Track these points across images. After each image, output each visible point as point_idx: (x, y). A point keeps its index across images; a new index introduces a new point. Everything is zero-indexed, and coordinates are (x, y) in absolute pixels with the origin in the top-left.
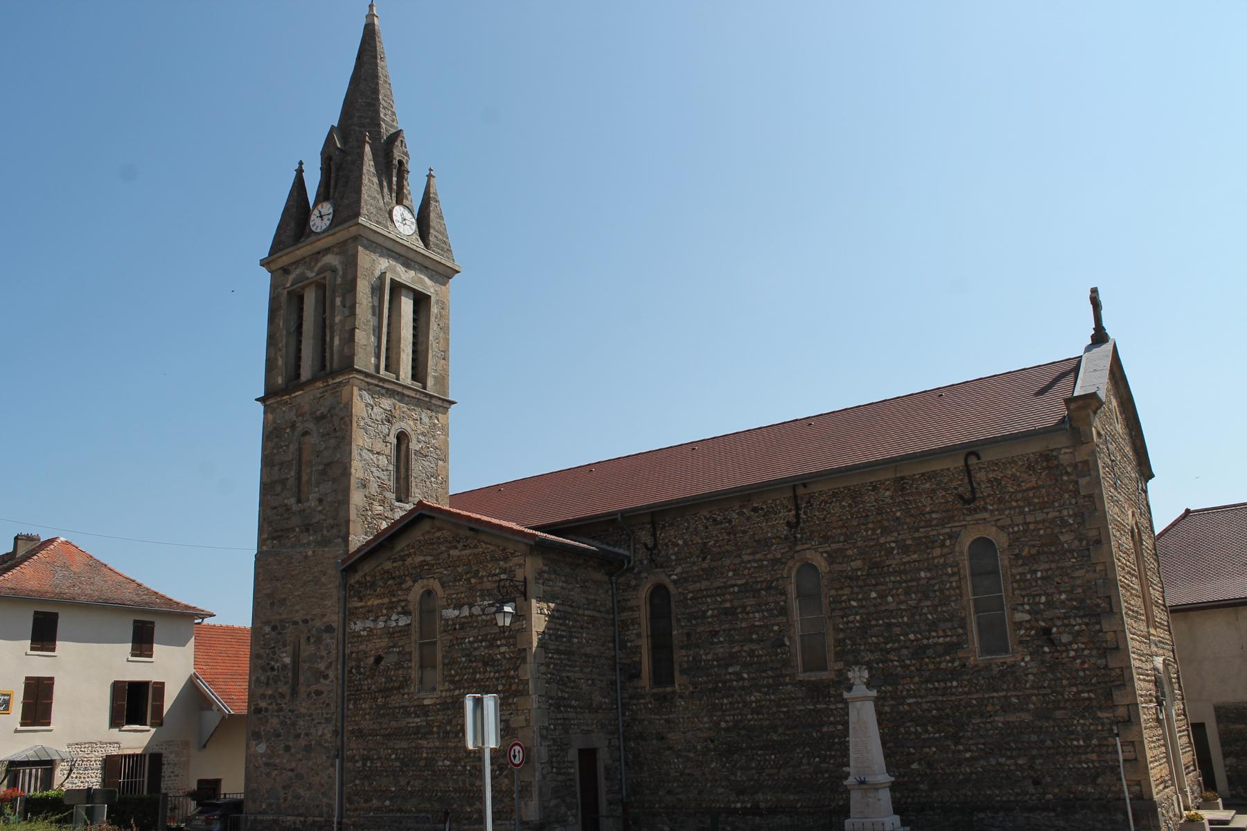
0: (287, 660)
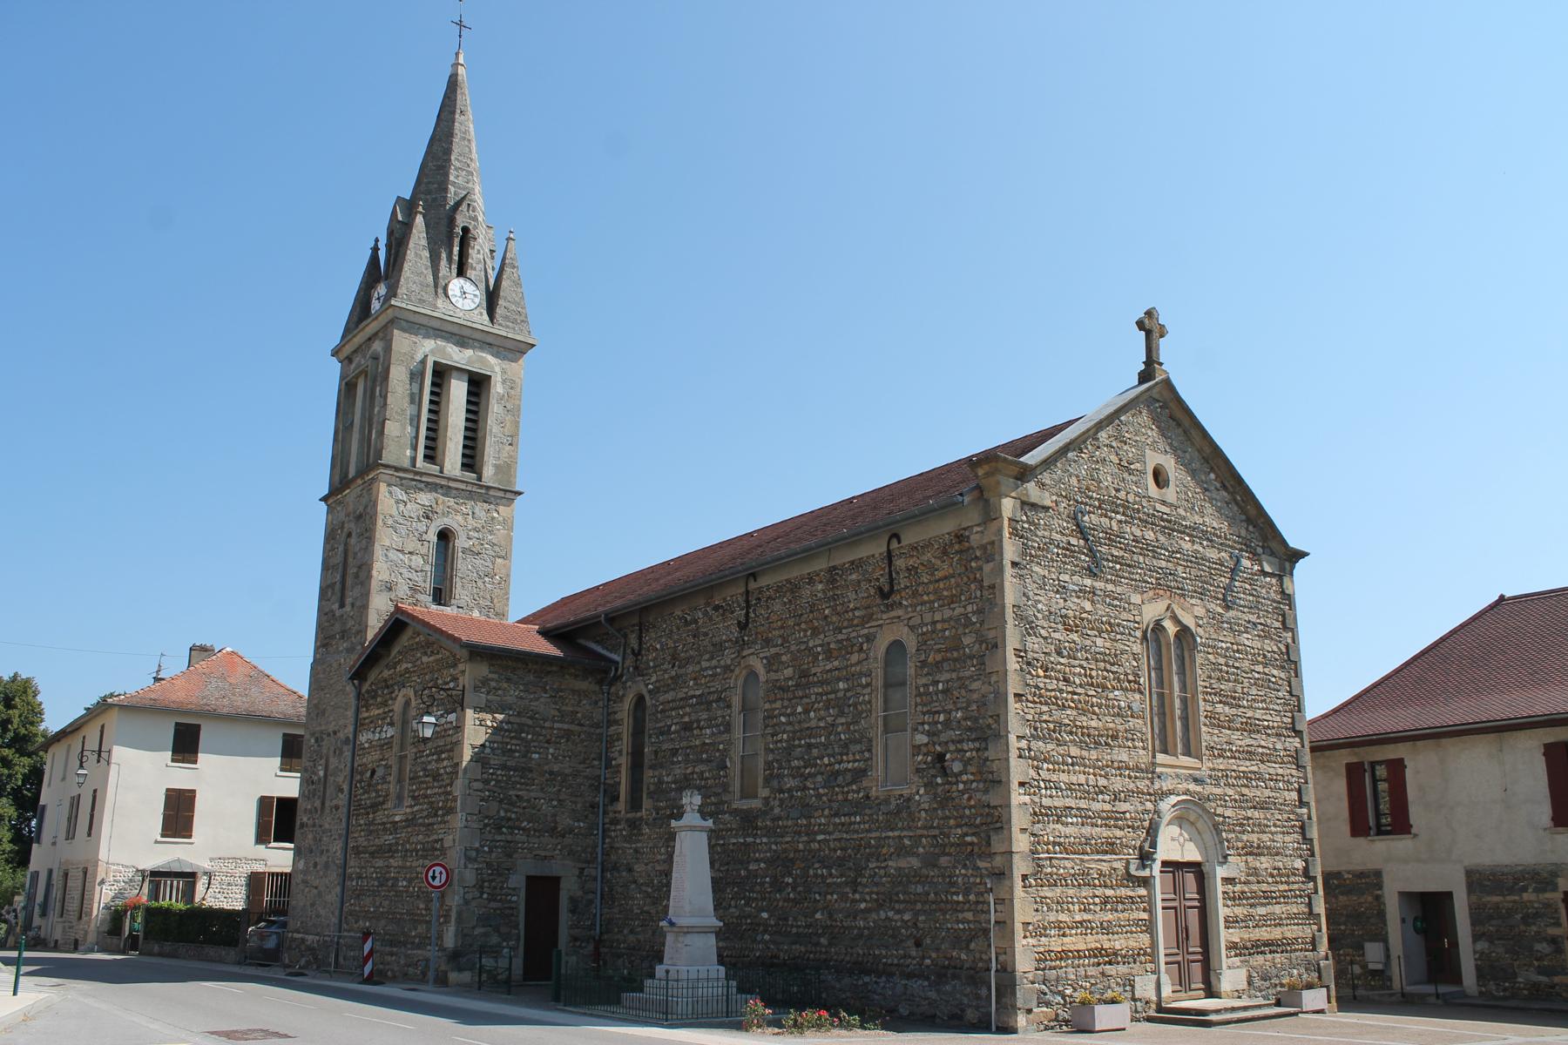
0: (321, 773)
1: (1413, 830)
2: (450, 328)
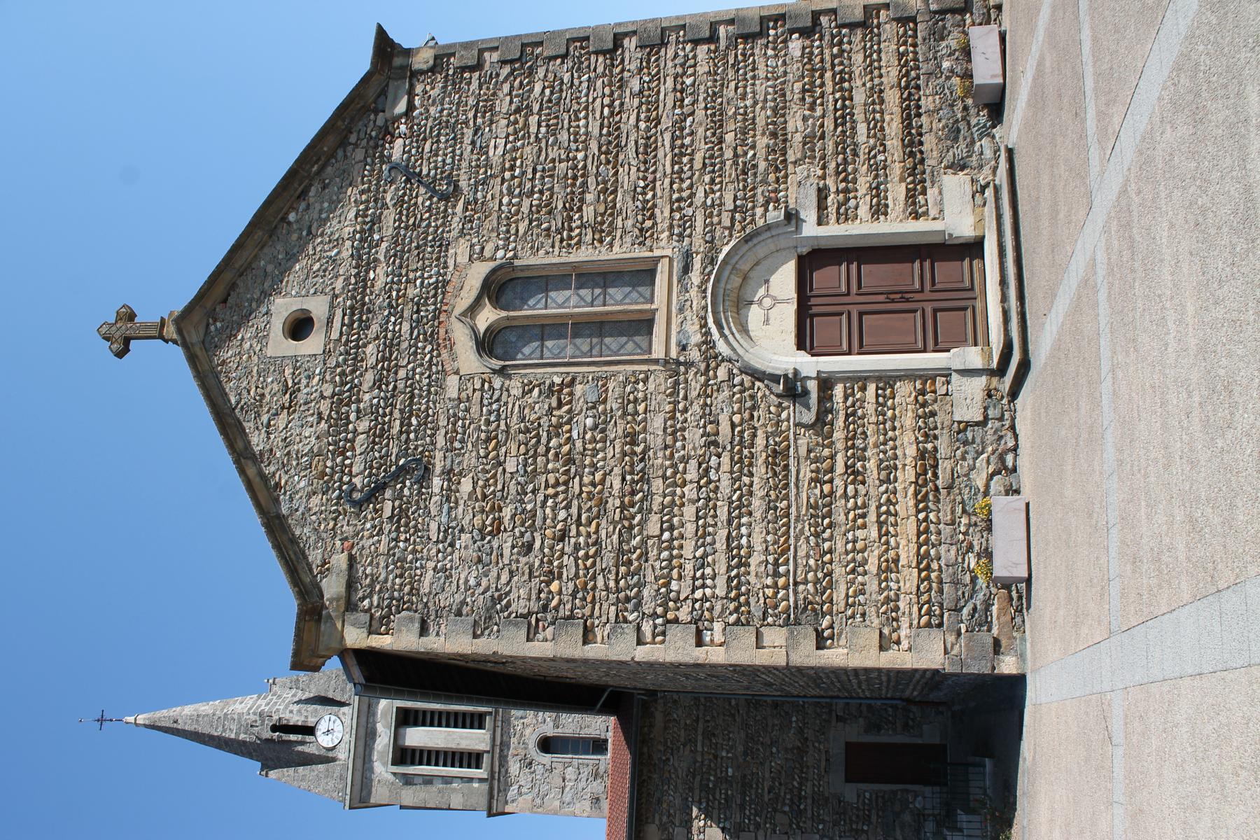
2: (361, 749)
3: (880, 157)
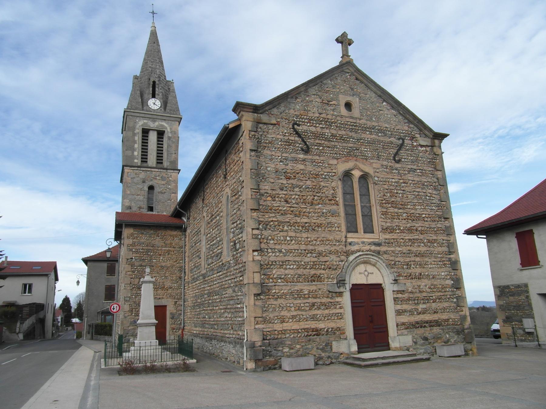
1: (541, 263)
3: (416, 313)
